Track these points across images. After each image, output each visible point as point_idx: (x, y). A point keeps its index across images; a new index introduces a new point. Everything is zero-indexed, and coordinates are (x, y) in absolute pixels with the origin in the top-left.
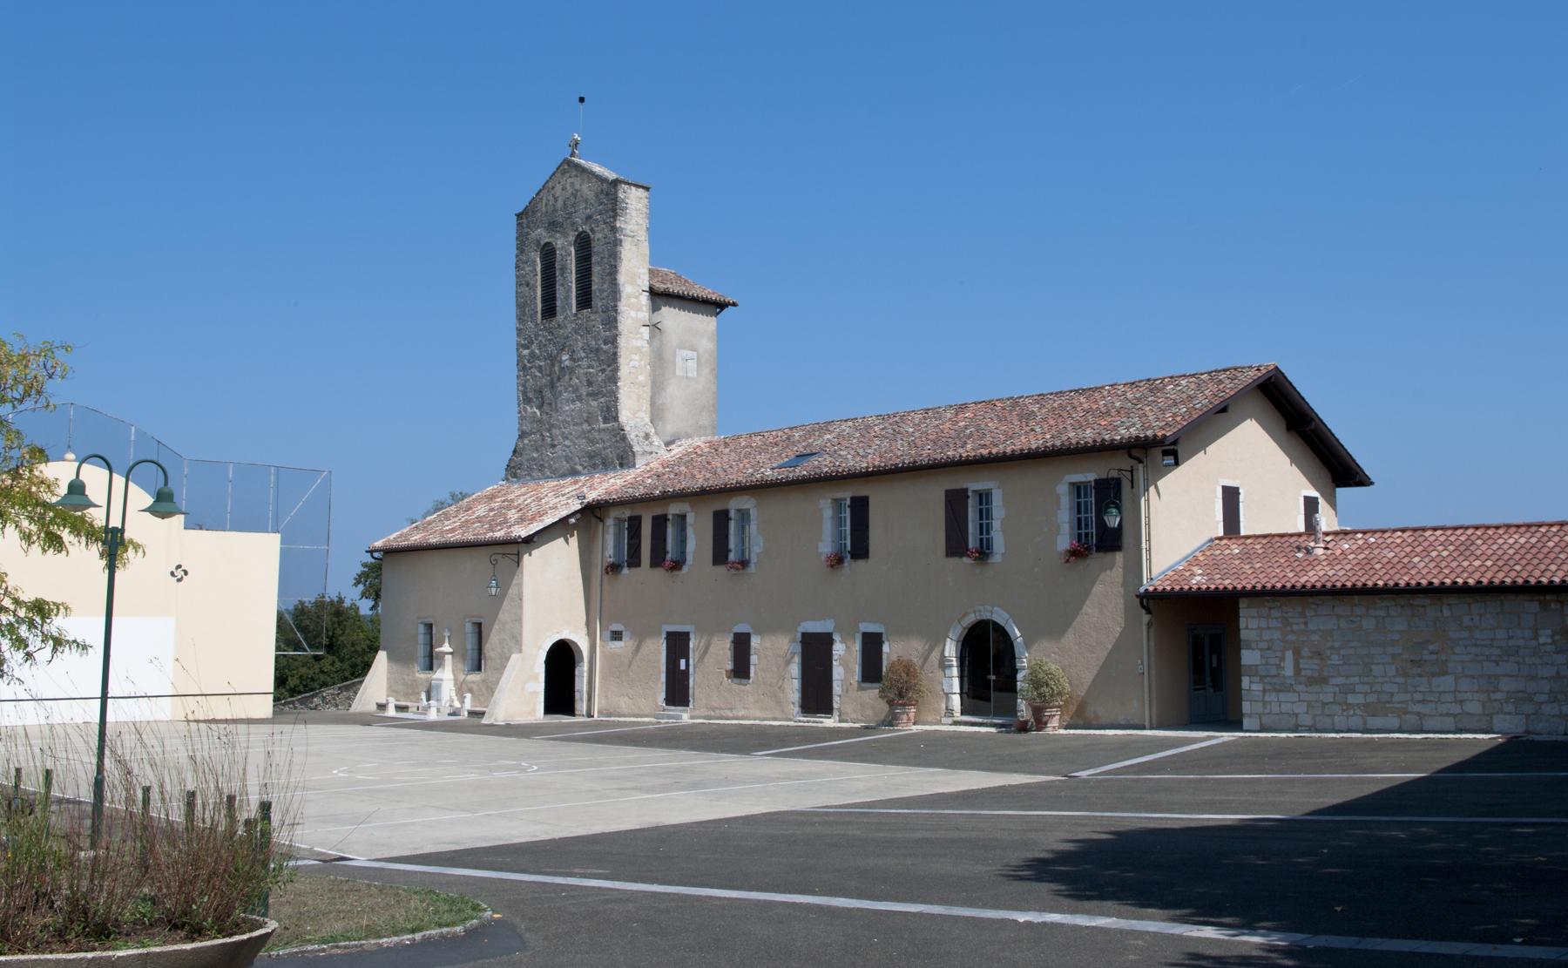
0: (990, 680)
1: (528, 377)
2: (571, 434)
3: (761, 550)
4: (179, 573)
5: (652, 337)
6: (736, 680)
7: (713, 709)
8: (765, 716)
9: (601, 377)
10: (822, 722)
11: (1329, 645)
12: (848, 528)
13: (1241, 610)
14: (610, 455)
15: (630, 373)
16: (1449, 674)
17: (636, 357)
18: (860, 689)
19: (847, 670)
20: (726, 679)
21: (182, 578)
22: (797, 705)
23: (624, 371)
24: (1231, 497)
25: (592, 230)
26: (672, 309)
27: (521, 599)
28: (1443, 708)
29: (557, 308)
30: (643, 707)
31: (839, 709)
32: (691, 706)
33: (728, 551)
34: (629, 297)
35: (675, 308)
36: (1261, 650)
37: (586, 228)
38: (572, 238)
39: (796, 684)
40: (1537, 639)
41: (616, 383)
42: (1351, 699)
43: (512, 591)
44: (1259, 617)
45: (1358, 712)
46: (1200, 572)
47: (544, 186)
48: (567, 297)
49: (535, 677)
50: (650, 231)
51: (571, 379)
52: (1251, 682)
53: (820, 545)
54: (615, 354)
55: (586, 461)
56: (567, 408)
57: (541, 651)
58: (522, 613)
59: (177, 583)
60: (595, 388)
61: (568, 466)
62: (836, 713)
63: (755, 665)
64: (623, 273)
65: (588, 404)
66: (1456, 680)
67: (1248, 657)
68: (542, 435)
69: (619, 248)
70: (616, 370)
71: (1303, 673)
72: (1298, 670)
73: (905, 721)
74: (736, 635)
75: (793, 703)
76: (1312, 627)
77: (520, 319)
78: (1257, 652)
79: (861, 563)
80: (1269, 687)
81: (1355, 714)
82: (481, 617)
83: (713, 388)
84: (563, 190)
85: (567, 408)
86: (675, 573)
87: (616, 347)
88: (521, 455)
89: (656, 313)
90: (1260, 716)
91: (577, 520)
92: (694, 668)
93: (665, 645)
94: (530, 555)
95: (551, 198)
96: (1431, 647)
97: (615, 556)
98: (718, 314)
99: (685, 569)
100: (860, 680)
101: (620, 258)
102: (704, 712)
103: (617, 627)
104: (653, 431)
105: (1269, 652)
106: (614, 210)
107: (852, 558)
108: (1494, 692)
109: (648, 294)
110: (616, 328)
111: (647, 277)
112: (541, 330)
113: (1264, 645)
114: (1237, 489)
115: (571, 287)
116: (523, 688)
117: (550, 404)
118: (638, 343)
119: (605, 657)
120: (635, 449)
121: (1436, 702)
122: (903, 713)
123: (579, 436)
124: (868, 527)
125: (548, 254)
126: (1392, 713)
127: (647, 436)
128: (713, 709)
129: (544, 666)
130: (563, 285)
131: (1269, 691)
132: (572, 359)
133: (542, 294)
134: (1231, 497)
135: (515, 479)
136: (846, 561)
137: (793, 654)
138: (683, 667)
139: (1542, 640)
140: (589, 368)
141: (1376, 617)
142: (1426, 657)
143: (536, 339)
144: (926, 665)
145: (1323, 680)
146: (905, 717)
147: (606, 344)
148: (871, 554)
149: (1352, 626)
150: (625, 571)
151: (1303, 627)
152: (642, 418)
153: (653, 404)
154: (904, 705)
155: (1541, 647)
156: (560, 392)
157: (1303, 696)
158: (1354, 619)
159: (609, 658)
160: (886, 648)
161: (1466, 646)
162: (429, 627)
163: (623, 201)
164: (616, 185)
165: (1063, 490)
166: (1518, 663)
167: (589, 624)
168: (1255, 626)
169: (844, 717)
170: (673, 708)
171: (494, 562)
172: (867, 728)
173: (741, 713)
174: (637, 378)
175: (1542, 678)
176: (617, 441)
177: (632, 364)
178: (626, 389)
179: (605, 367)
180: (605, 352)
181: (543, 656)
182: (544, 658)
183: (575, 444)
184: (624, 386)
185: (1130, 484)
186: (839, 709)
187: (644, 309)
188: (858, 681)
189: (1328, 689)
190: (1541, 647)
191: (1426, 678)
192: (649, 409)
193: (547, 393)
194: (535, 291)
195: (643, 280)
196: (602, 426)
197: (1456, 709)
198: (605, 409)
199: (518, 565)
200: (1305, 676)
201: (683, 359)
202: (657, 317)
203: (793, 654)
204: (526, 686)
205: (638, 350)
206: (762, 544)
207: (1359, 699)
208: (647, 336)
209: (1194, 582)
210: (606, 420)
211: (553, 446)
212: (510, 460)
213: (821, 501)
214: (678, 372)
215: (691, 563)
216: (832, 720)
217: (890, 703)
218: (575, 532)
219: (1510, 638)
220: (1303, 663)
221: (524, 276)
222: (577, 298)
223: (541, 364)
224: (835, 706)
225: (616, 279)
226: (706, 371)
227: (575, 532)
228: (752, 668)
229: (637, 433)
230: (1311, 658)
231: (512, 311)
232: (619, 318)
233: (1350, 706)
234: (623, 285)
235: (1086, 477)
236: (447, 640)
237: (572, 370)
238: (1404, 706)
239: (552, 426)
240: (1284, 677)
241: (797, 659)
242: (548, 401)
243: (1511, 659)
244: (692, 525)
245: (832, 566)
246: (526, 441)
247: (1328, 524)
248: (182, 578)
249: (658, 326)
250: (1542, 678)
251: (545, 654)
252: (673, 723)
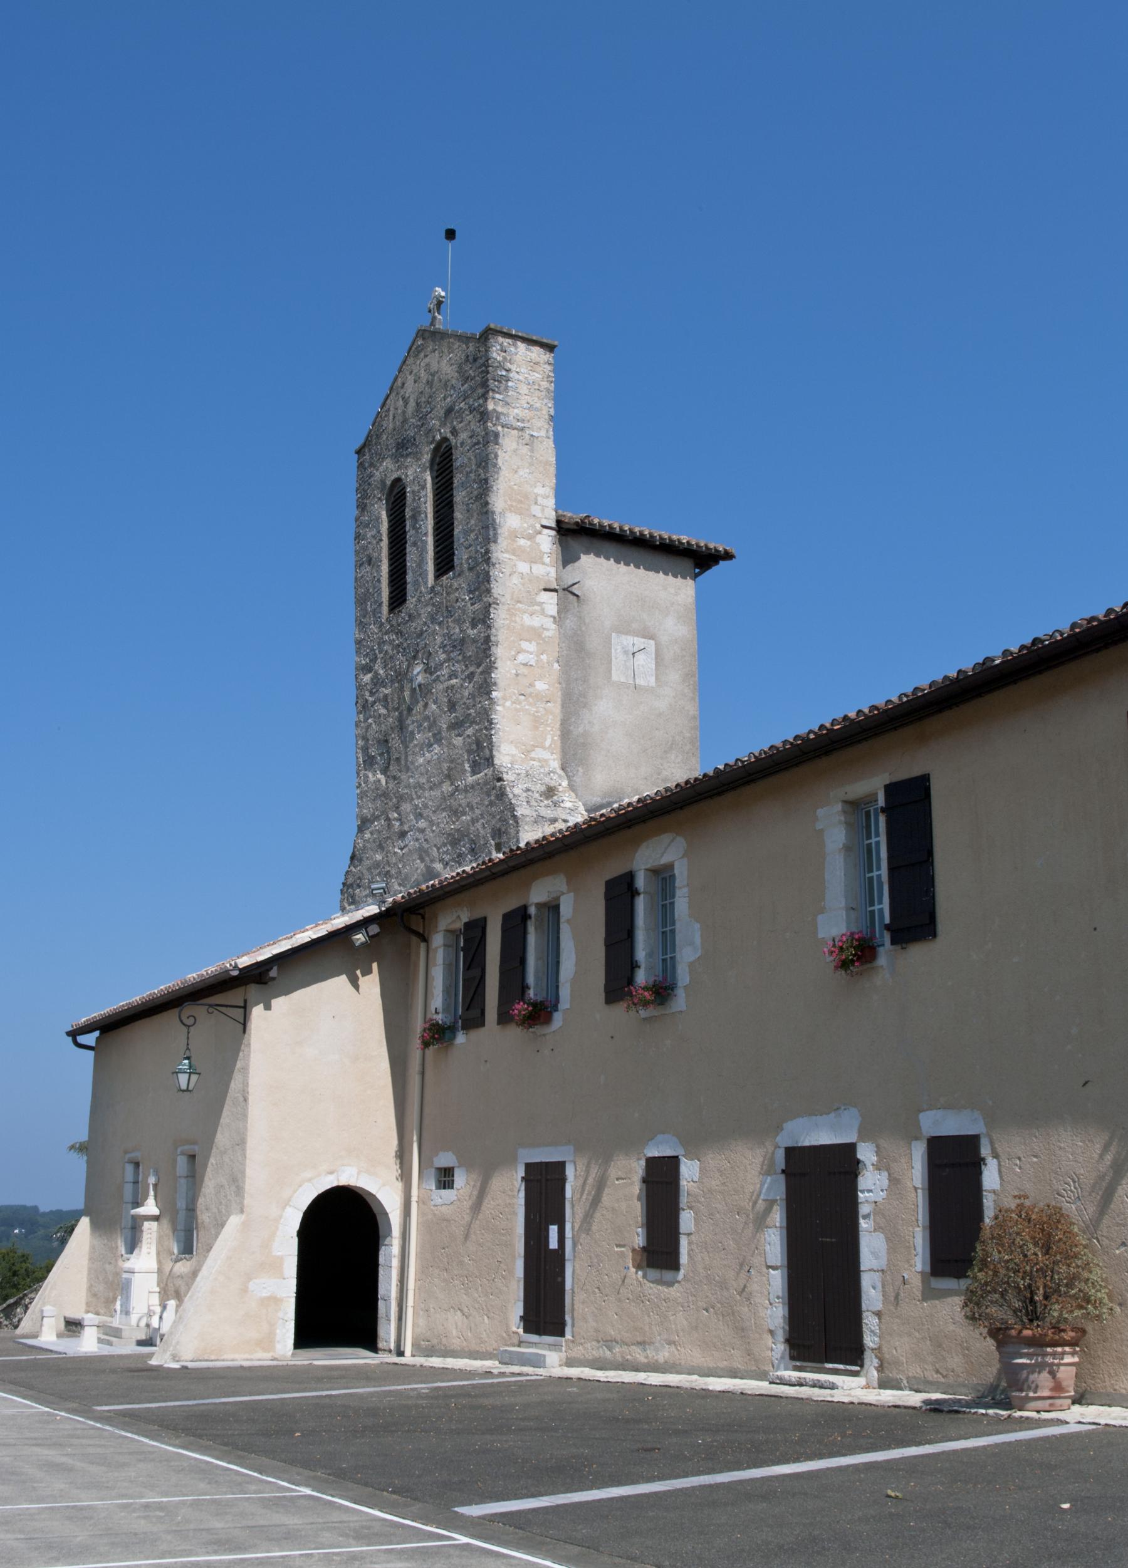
1: (370, 721)
2: (425, 806)
3: (699, 954)
5: (563, 609)
6: (653, 1273)
7: (609, 1343)
8: (712, 1365)
9: (469, 687)
10: (833, 1387)
12: (883, 871)
14: (482, 832)
15: (517, 675)
17: (531, 647)
18: (929, 1294)
19: (896, 1242)
20: (633, 1270)
22: (781, 1336)
23: (505, 670)
26: (602, 560)
27: (245, 1100)
29: (409, 586)
30: (484, 1335)
31: (878, 1351)
32: (568, 1336)
33: (634, 966)
34: (514, 535)
35: (608, 559)
37: (446, 431)
38: (426, 458)
39: (777, 1281)
41: (489, 693)
43: (235, 1085)
47: (391, 389)
48: (421, 562)
49: (274, 1266)
50: (558, 421)
51: (426, 705)
54: (487, 639)
55: (446, 853)
56: (421, 760)
57: (289, 1210)
58: (246, 1128)
60: (459, 713)
61: (422, 866)
62: (871, 1361)
63: (689, 1234)
64: (501, 491)
65: (450, 745)
68: (388, 819)
69: (491, 447)
70: (490, 668)
73: (1046, 1393)
74: (651, 1162)
75: (771, 1332)
77: (361, 625)
79: (918, 953)
82: (195, 1143)
83: (692, 709)
84: (415, 382)
85: (421, 760)
86: (538, 1030)
87: (489, 627)
88: (361, 860)
89: (569, 567)
91: (371, 937)
92: (575, 1245)
93: (522, 1194)
94: (268, 1007)
95: (401, 402)
97: (446, 1010)
98: (696, 576)
99: (558, 1019)
100: (928, 1269)
101: (495, 465)
102: (593, 1350)
103: (445, 1159)
104: (565, 783)
106: (484, 384)
107: (893, 943)
109: (553, 533)
110: (489, 591)
111: (551, 502)
112: (386, 633)
115: (426, 542)
116: (245, 1290)
117: (398, 759)
118: (536, 622)
119: (427, 1227)
120: (519, 812)
122: (1039, 1367)
123: (438, 808)
124: (930, 853)
125: (397, 497)
127: (550, 792)
128: (609, 1343)
129: (295, 1241)
130: (415, 544)
132: (428, 670)
133: (390, 571)
135: (352, 907)
136: (881, 950)
137: (771, 1203)
138: (553, 1244)
140: (450, 678)
143: (380, 652)
144: (1106, 1221)
146: (1043, 1379)
147: (474, 626)
148: (941, 927)
150: (461, 1038)
152: (546, 761)
154: (1038, 1343)
156: (412, 733)
159: (434, 1226)
160: (990, 1178)
163: (500, 366)
164: (487, 339)
167: (402, 1155)
169: (893, 1374)
170: (534, 1338)
171: (190, 1021)
172: (935, 1408)
173: (664, 1354)
174: (531, 685)
176: (491, 804)
177: (521, 658)
178: (508, 704)
179: (472, 669)
180: (474, 641)
181: (293, 1220)
183: (432, 823)
184: (505, 699)
186: (878, 1351)
187: (547, 560)
188: (922, 1273)
192: (559, 743)
193: (395, 742)
194: (379, 570)
195: (543, 508)
196: (470, 779)
198: (474, 747)
199: (244, 1032)
201: (626, 652)
202: (572, 574)
203: (771, 1203)
204: (251, 1286)
205: (535, 634)
206: (698, 940)
208: (552, 610)
210: (476, 768)
211: (403, 835)
212: (347, 872)
213: (820, 812)
214: (616, 676)
215: (568, 1006)
216: (861, 1381)
217: (999, 1334)
218: (375, 966)
221: (365, 548)
222: (436, 559)
223: (386, 692)
224: (870, 1341)
225: (487, 503)
226: (674, 676)
227: (375, 966)
228: (684, 1242)
229: (529, 785)
231: (350, 611)
232: (494, 573)
234: (502, 513)
236: (152, 1193)
237: (424, 690)
239: (401, 798)
241: (778, 1217)
242: (396, 755)
244: (568, 921)
245: (844, 965)
246: (367, 836)
249: (575, 589)
251: (301, 1215)
252: (513, 1374)
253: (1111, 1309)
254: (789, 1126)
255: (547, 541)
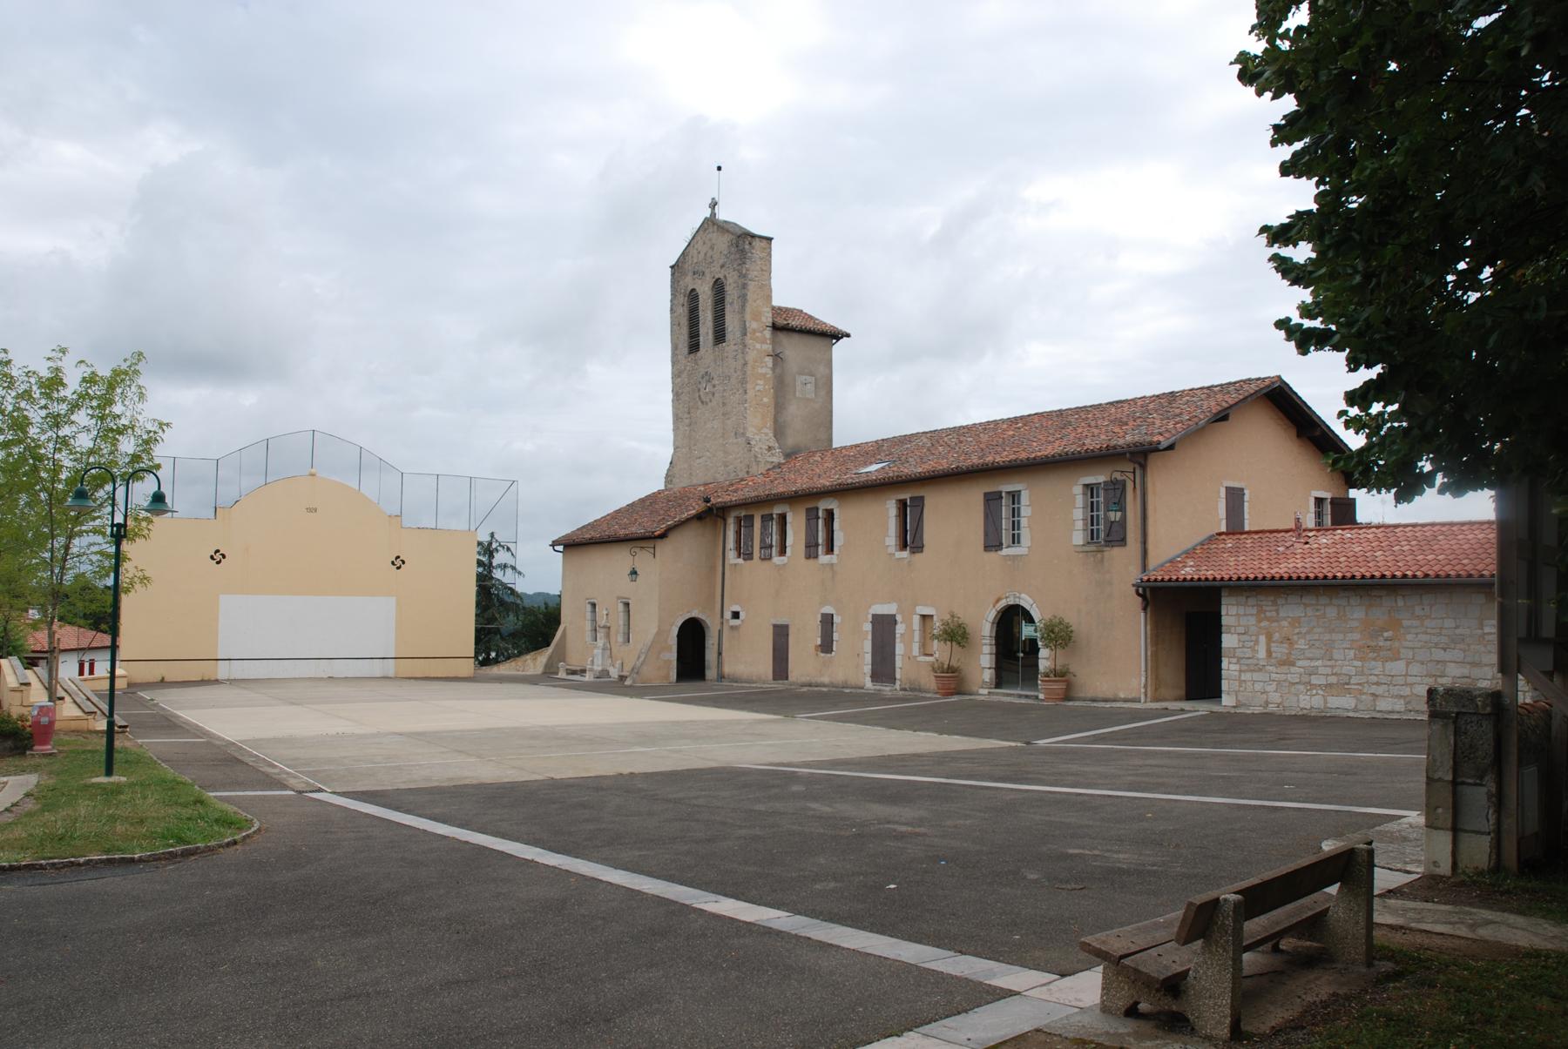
0: (1018, 657)
4: (398, 563)
5: (775, 364)
11: (1297, 631)
13: (1223, 599)
16: (1402, 659)
21: (220, 561)
24: (1235, 498)
25: (725, 277)
28: (1395, 690)
34: (754, 331)
36: (1239, 634)
40: (1482, 629)
42: (1315, 680)
44: (1237, 605)
45: (1320, 692)
46: (1192, 563)
52: (1230, 663)
53: (887, 539)
59: (217, 565)
66: (1408, 664)
67: (1228, 641)
71: (1274, 655)
72: (1269, 653)
76: (1282, 614)
78: (1235, 636)
80: (1244, 668)
81: (1317, 694)
90: (1237, 693)
96: (1386, 634)
105: (1244, 636)
108: (1440, 676)
113: (1241, 630)
114: (1242, 490)
118: (763, 371)
121: (1389, 685)
125: (693, 297)
126: (1350, 694)
129: (676, 639)
131: (1244, 671)
134: (1235, 498)
139: (1487, 630)
141: (1339, 606)
142: (1381, 644)
145: (1288, 662)
149: (1318, 614)
151: (1274, 614)
153: (776, 421)
155: (1486, 637)
157: (1274, 676)
158: (1319, 607)
161: (1417, 634)
162: (594, 605)
165: (1078, 490)
166: (1464, 651)
168: (1234, 613)
174: (762, 400)
175: (1486, 665)
181: (675, 631)
182: (676, 633)
185: (1132, 484)
187: (768, 342)
189: (1293, 669)
190: (1486, 637)
191: (1380, 663)
197: (1406, 691)
200: (1276, 658)
201: (802, 383)
207: (1322, 681)
208: (770, 365)
209: (1183, 572)
213: (888, 502)
219: (1457, 627)
220: (1274, 647)
230: (1282, 642)
233: (1314, 686)
235: (1097, 479)
238: (1360, 687)
240: (1258, 659)
243: (1458, 646)
247: (1250, 524)
248: (220, 561)
249: (780, 355)
250: (1486, 665)
251: (678, 629)
253: (88, 430)
254: (874, 607)
255: (768, 333)
